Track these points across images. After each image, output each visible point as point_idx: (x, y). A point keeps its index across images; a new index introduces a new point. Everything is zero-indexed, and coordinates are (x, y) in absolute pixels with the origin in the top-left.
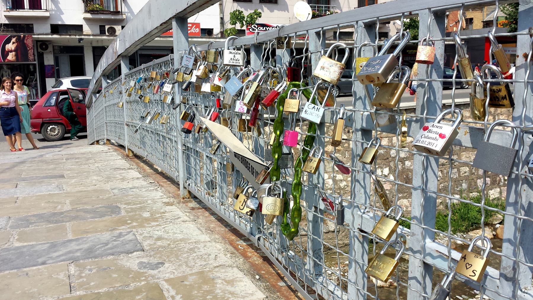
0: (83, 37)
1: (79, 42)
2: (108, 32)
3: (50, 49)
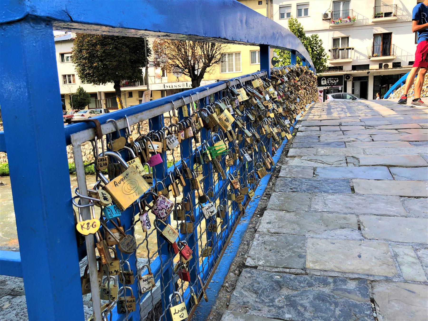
0: (369, 71)
1: (368, 74)
2: (384, 67)
3: (351, 78)
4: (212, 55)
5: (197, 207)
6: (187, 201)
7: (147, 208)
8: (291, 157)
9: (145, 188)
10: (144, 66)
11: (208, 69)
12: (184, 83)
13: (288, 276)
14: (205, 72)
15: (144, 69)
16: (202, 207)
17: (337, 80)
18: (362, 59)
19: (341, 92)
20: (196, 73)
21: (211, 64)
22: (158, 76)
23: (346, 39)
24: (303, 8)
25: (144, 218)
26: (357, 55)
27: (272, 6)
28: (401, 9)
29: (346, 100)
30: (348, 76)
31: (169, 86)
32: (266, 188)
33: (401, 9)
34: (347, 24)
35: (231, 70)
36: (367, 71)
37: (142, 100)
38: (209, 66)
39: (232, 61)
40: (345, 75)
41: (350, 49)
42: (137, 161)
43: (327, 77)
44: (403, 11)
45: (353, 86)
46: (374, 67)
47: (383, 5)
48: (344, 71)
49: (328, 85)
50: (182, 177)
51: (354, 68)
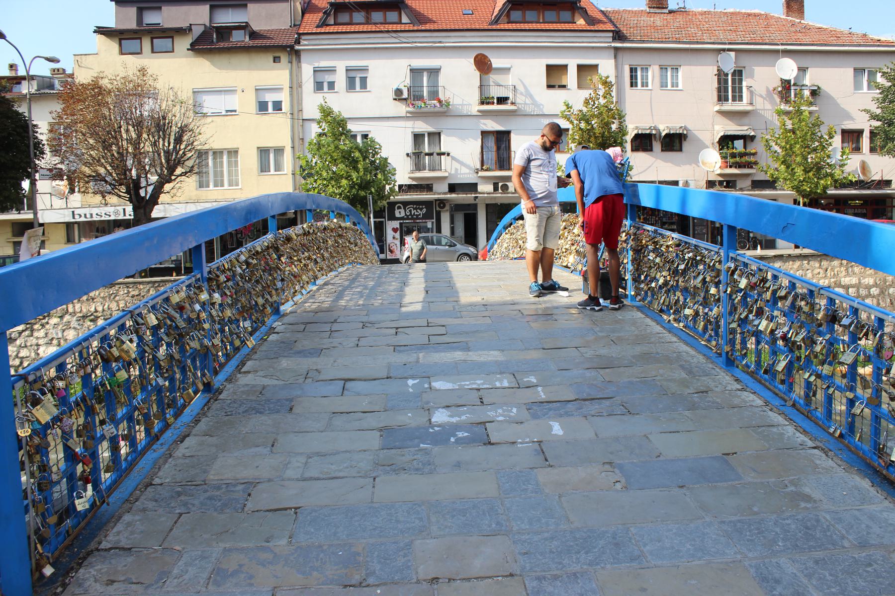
2: (502, 190)
3: (447, 207)
4: (175, 160)
5: (98, 428)
6: (88, 423)
7: (56, 426)
8: (245, 372)
9: (55, 412)
10: (29, 176)
11: (167, 187)
12: (118, 208)
13: (188, 487)
14: (162, 193)
15: (26, 184)
16: (103, 429)
17: (422, 208)
18: (465, 174)
19: (432, 232)
20: (142, 193)
21: (173, 178)
22: (60, 194)
23: (435, 136)
24: (359, 75)
25: (54, 431)
26: (456, 165)
27: (299, 67)
28: (521, 94)
29: (438, 247)
30: (442, 203)
31: (85, 215)
32: (199, 414)
33: (521, 94)
34: (436, 110)
35: (219, 183)
36: (473, 195)
37: (20, 242)
38: (169, 181)
39: (222, 166)
40: (436, 200)
41: (444, 154)
42: (49, 395)
43: (405, 204)
44: (526, 97)
45: (452, 221)
46: (485, 188)
47: (493, 84)
48: (434, 194)
49: (408, 219)
50: (82, 405)
51: (453, 188)
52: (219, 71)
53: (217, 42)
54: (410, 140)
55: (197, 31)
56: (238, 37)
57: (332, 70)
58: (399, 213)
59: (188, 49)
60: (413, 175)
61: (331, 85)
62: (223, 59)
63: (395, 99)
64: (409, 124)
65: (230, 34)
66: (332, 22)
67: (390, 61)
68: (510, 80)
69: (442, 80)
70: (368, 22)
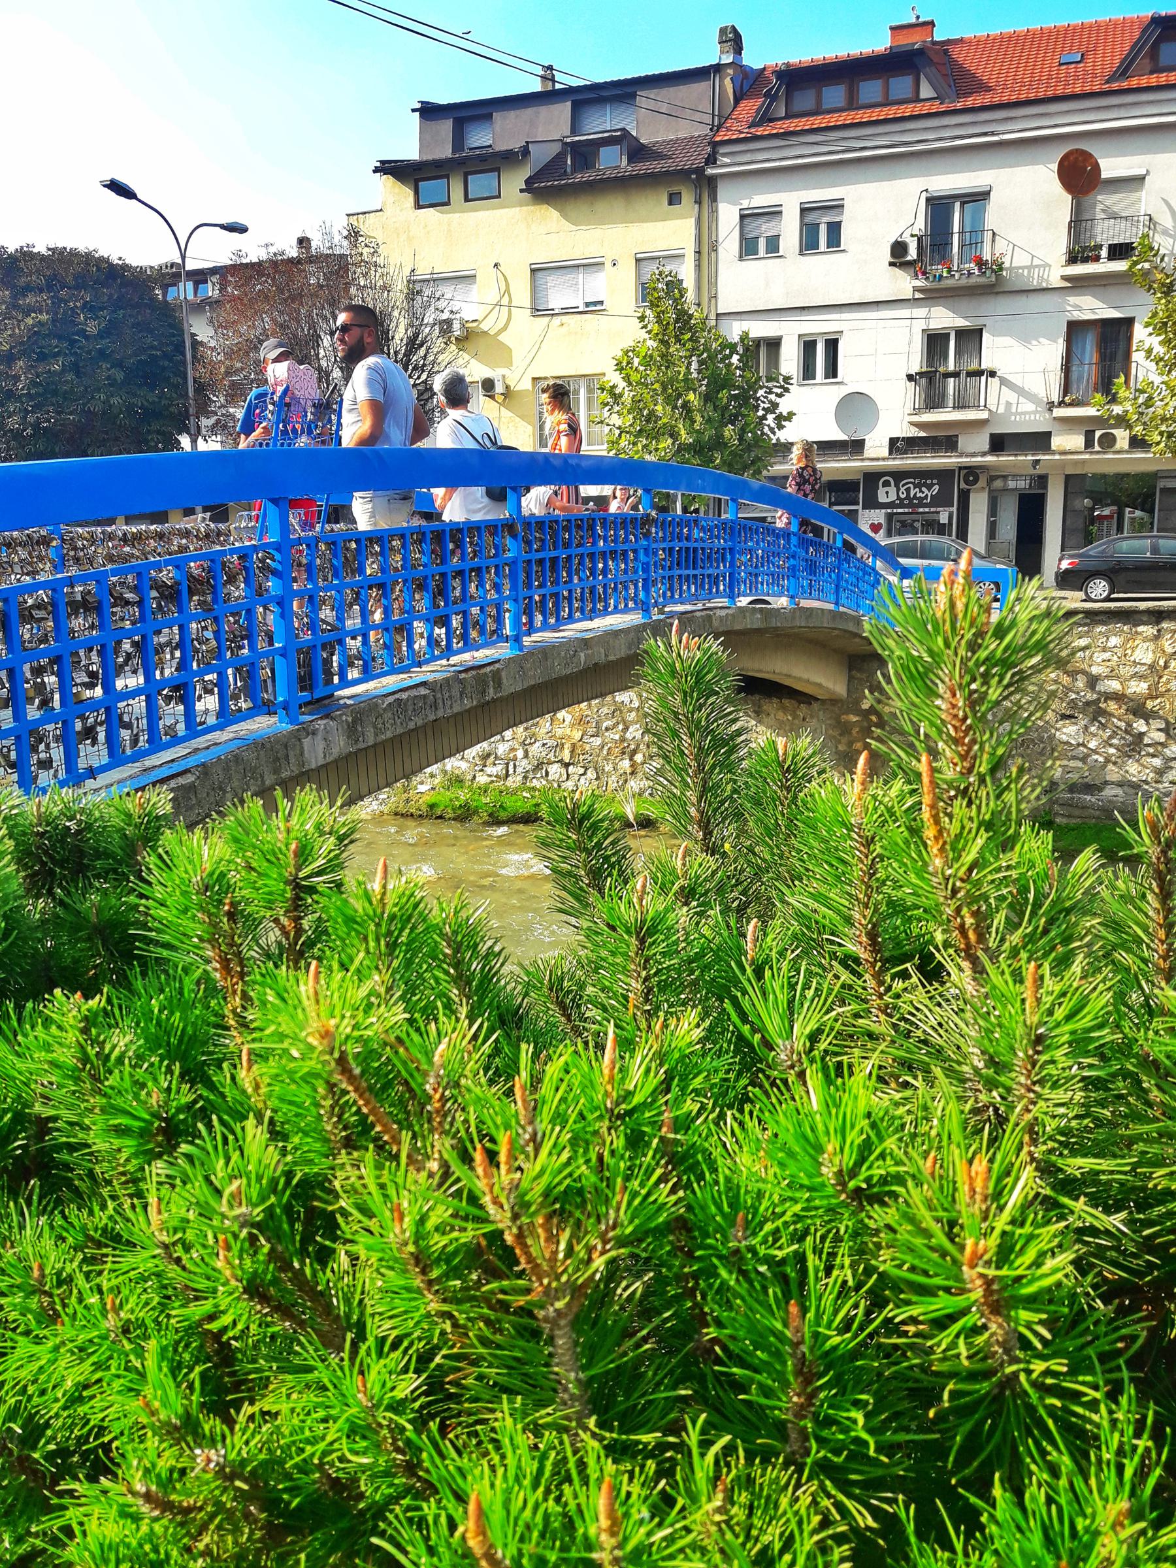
3: (982, 482)
17: (933, 485)
18: (1025, 413)
23: (970, 338)
26: (1008, 395)
27: (714, 211)
30: (971, 473)
34: (973, 280)
36: (1030, 458)
43: (899, 476)
45: (993, 511)
46: (1068, 442)
48: (961, 456)
49: (901, 506)
51: (999, 443)
52: (574, 228)
53: (574, 171)
54: (918, 347)
55: (541, 155)
56: (612, 160)
57: (774, 213)
58: (886, 494)
59: (522, 191)
60: (916, 419)
61: (773, 245)
62: (580, 207)
63: (891, 264)
64: (921, 312)
65: (596, 155)
66: (782, 113)
67: (885, 184)
68: (1147, 201)
69: (994, 215)
70: (852, 104)
